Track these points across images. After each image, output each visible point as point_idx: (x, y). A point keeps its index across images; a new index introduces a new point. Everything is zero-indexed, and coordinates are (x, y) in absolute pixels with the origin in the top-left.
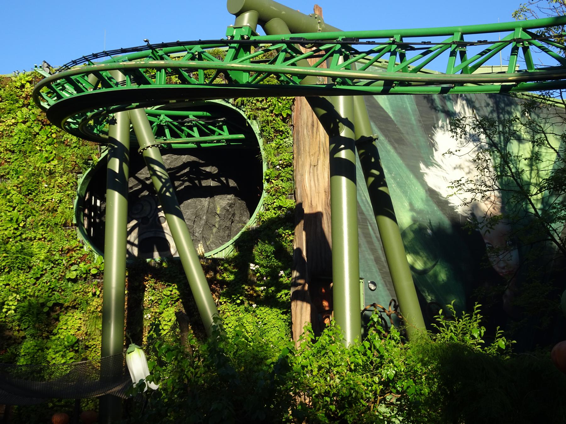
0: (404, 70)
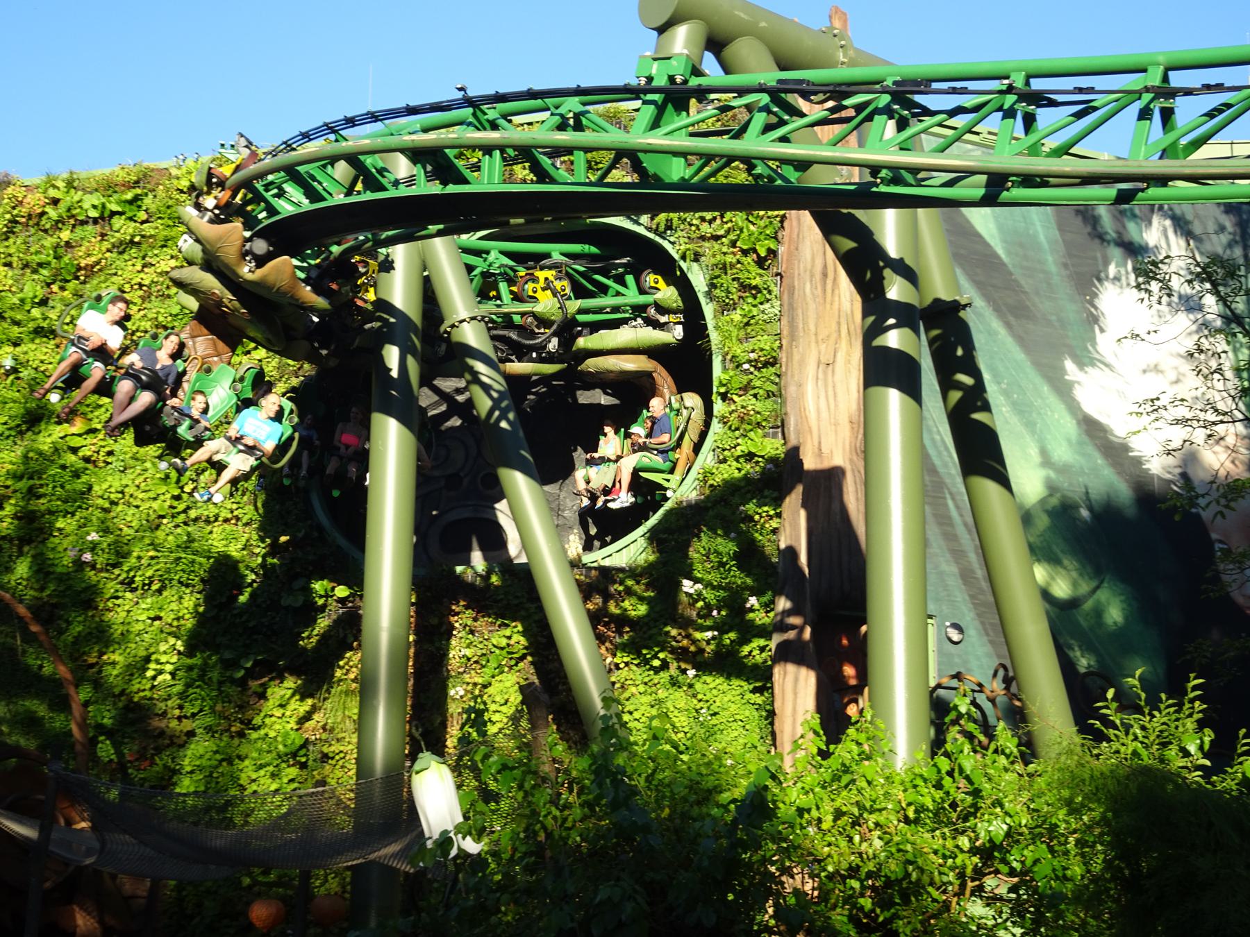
0: (1034, 150)
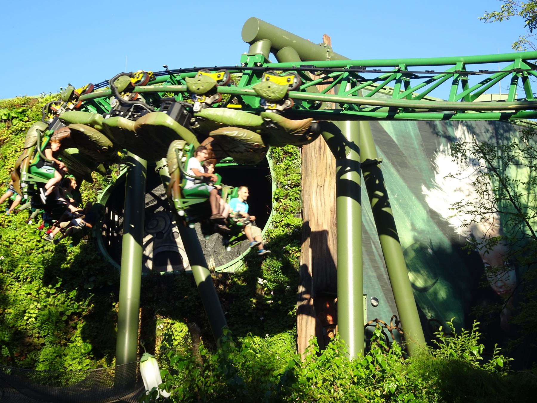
0: (409, 97)
